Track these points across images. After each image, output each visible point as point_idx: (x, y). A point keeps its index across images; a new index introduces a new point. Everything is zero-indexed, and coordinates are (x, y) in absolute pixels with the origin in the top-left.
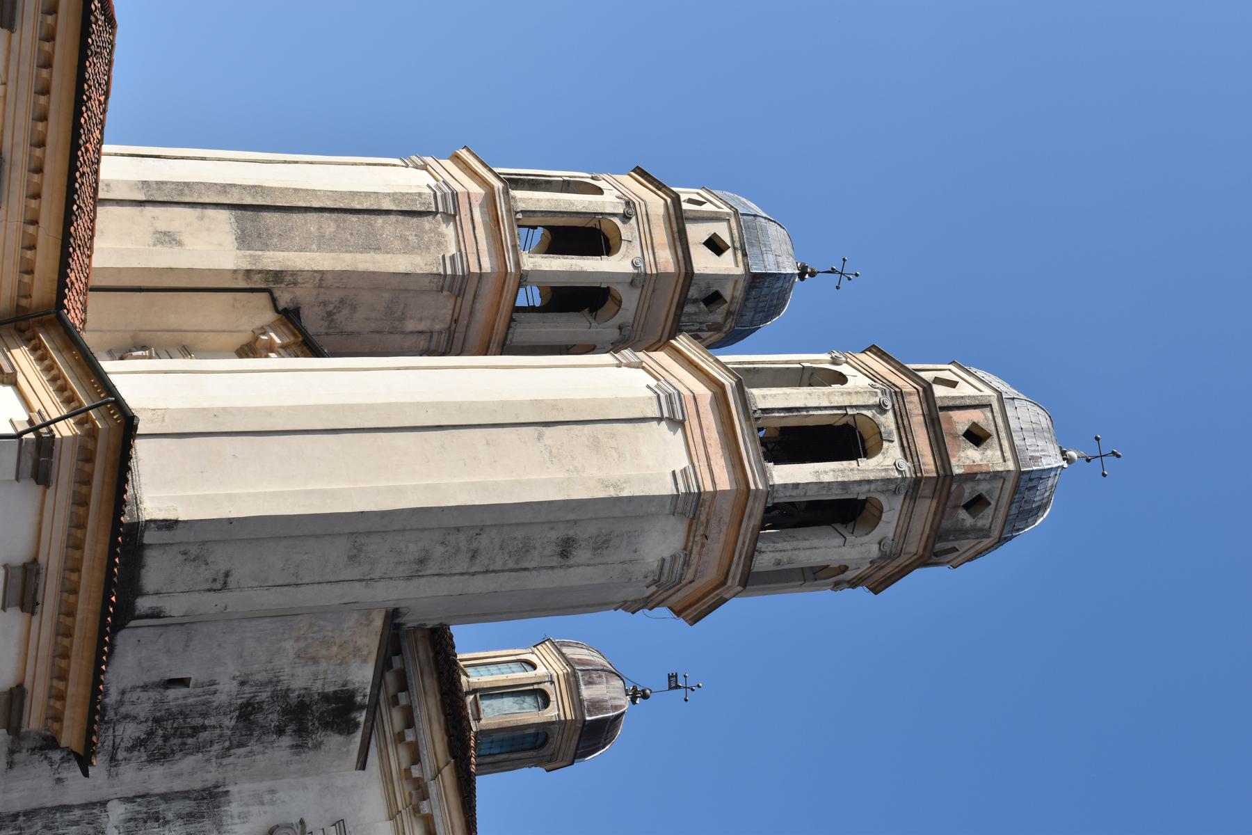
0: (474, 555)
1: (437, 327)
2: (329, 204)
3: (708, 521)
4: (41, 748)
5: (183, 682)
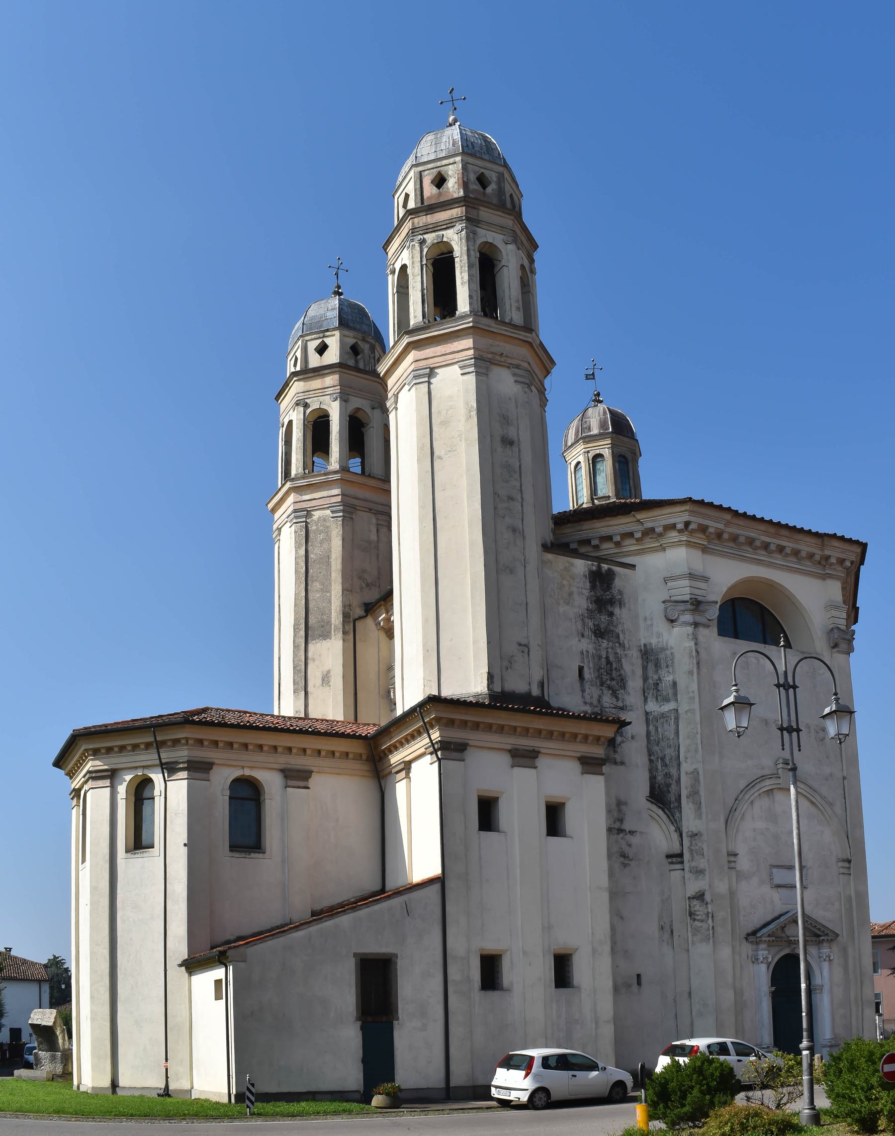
2: (303, 586)
3: (492, 353)
4: (614, 747)
5: (581, 669)
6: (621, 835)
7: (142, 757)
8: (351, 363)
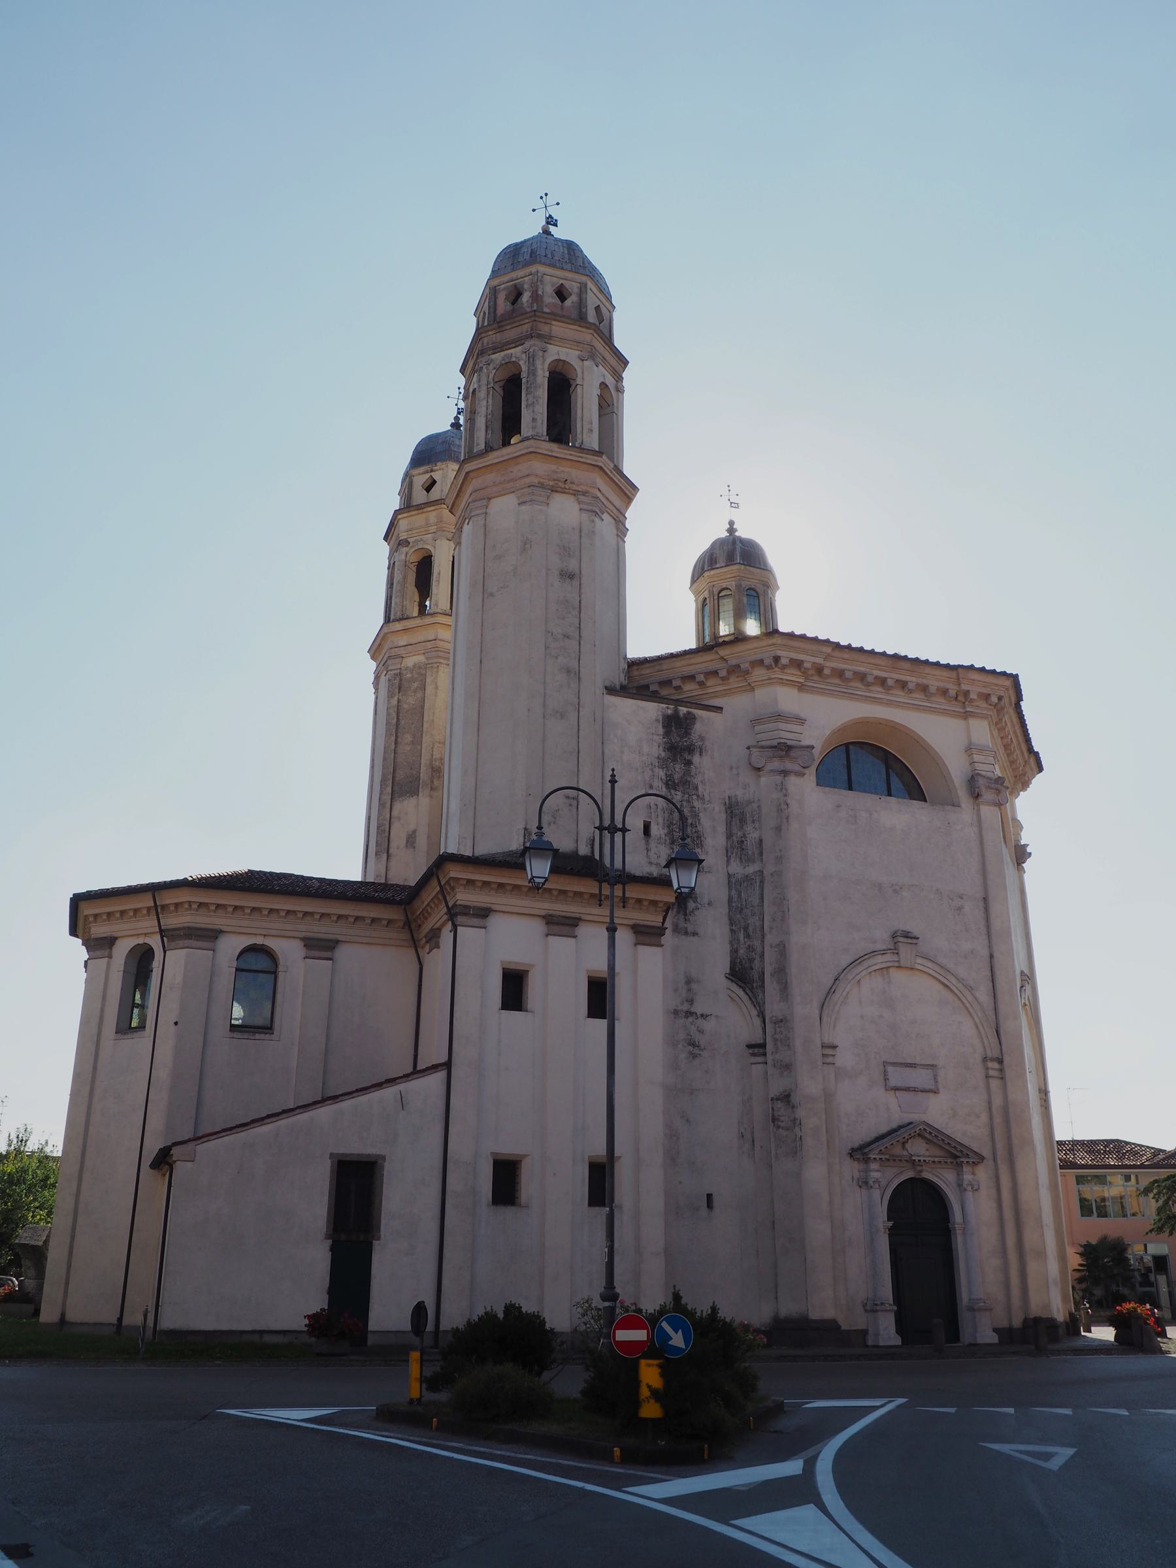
2: (393, 738)
6: (691, 1019)
7: (246, 923)
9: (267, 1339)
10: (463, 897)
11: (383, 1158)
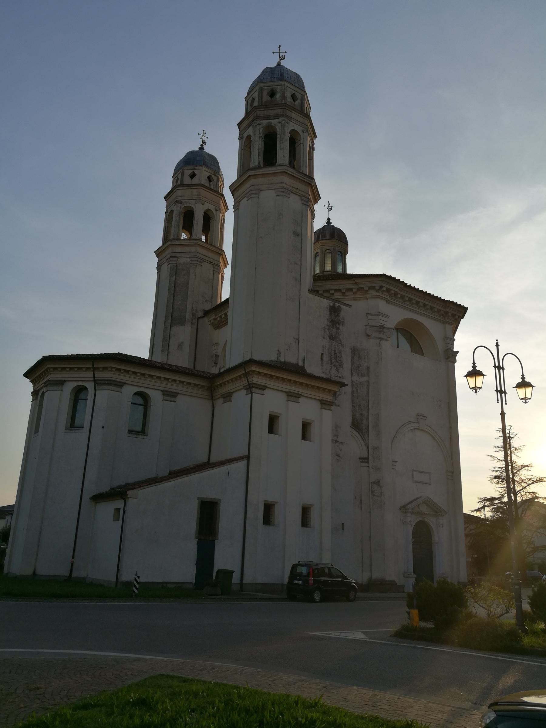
0: (296, 263)
1: (212, 269)
2: (172, 296)
3: (293, 187)
4: (336, 397)
5: (322, 354)
6: (337, 444)
8: (207, 185)
9: (169, 586)
10: (256, 379)
11: (220, 500)
